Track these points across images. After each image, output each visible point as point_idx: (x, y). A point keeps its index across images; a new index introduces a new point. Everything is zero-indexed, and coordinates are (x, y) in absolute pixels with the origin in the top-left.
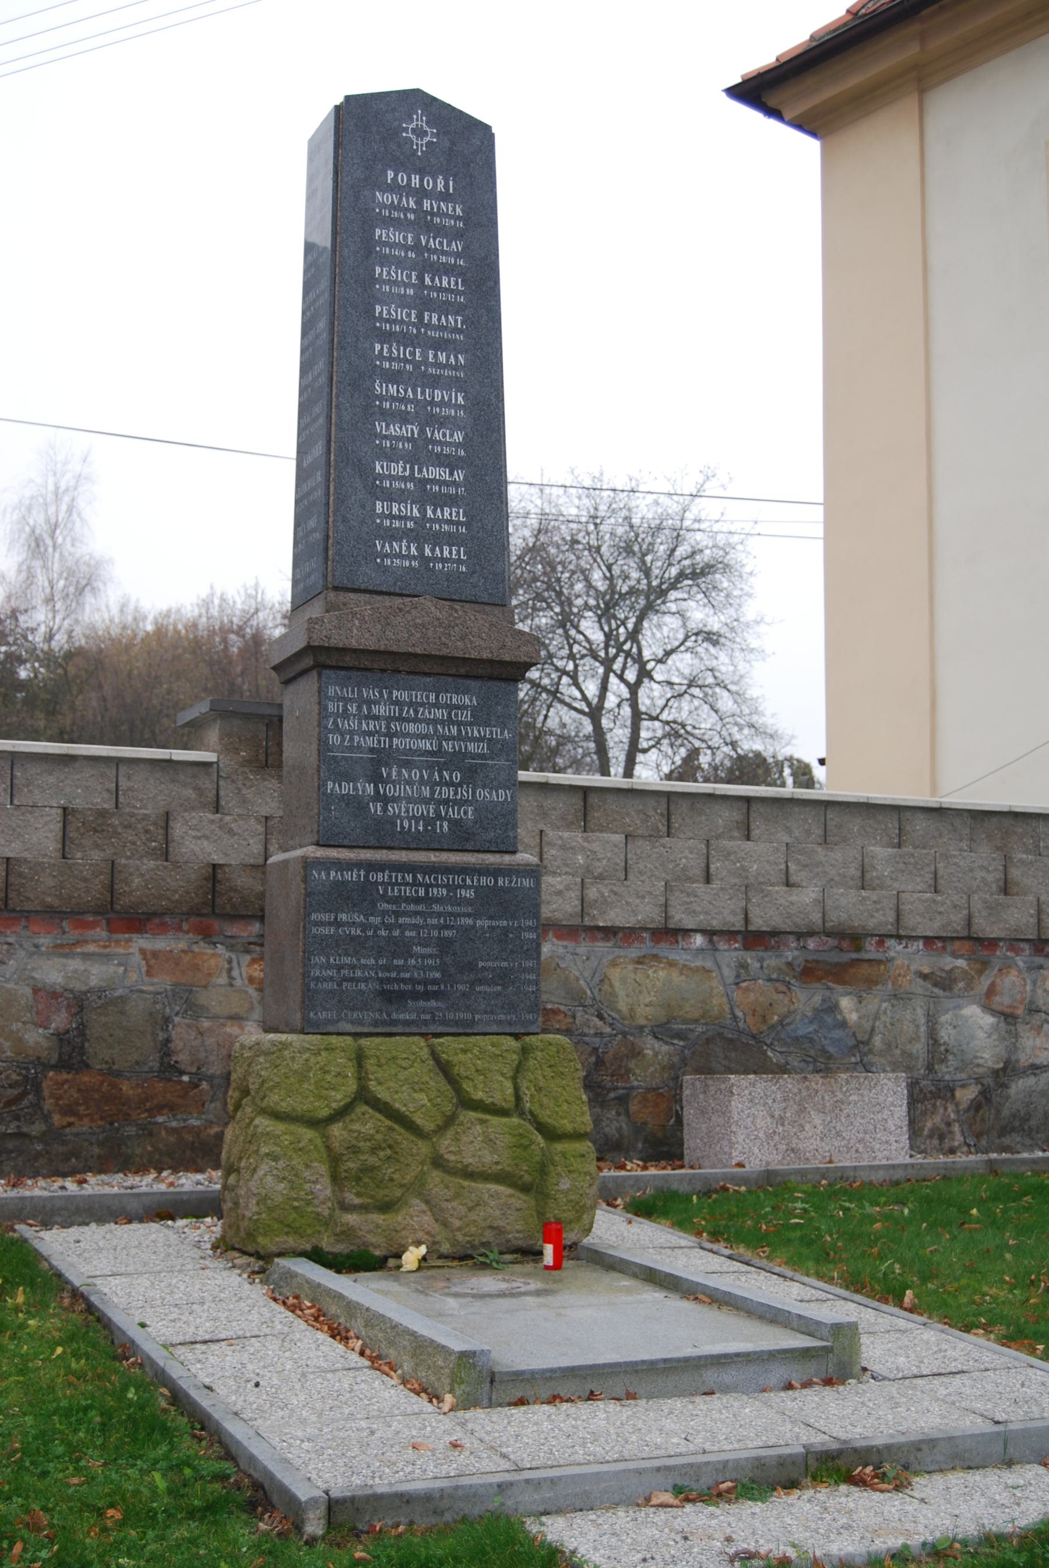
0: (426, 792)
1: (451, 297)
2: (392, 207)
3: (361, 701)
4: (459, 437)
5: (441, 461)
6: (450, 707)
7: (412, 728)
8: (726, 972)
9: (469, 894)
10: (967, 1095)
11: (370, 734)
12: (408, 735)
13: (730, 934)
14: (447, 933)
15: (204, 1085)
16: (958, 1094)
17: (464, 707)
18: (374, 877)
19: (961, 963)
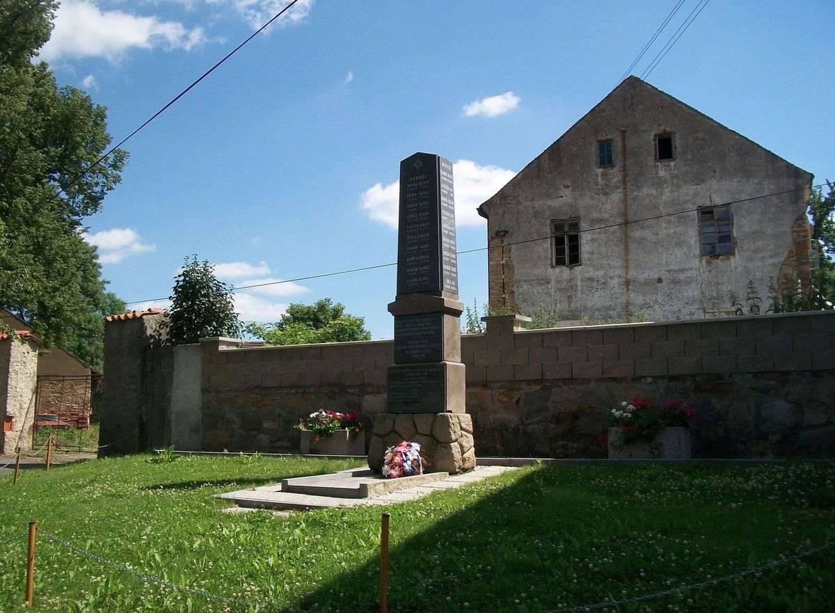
0: (419, 347)
1: (426, 207)
2: (412, 187)
3: (403, 324)
4: (427, 246)
5: (424, 253)
6: (425, 322)
7: (415, 329)
8: (662, 391)
9: (426, 374)
10: (774, 438)
11: (405, 332)
12: (414, 331)
13: (663, 377)
14: (421, 385)
15: (486, 432)
16: (770, 437)
17: (428, 322)
18: (405, 371)
19: (772, 383)
